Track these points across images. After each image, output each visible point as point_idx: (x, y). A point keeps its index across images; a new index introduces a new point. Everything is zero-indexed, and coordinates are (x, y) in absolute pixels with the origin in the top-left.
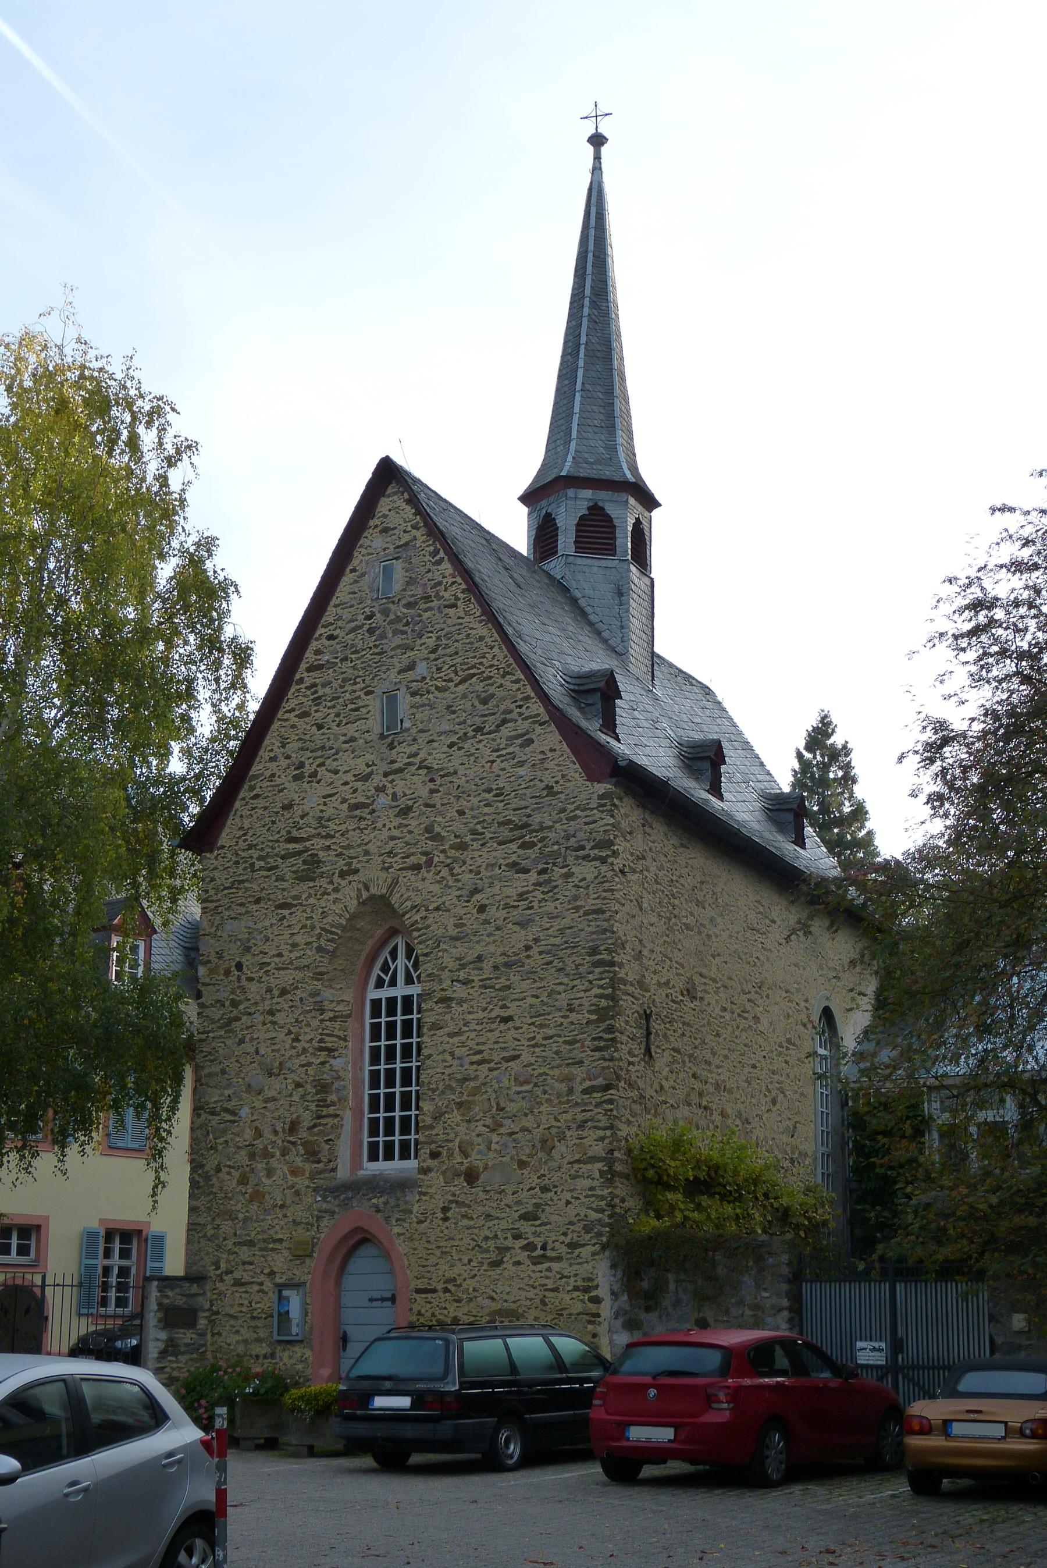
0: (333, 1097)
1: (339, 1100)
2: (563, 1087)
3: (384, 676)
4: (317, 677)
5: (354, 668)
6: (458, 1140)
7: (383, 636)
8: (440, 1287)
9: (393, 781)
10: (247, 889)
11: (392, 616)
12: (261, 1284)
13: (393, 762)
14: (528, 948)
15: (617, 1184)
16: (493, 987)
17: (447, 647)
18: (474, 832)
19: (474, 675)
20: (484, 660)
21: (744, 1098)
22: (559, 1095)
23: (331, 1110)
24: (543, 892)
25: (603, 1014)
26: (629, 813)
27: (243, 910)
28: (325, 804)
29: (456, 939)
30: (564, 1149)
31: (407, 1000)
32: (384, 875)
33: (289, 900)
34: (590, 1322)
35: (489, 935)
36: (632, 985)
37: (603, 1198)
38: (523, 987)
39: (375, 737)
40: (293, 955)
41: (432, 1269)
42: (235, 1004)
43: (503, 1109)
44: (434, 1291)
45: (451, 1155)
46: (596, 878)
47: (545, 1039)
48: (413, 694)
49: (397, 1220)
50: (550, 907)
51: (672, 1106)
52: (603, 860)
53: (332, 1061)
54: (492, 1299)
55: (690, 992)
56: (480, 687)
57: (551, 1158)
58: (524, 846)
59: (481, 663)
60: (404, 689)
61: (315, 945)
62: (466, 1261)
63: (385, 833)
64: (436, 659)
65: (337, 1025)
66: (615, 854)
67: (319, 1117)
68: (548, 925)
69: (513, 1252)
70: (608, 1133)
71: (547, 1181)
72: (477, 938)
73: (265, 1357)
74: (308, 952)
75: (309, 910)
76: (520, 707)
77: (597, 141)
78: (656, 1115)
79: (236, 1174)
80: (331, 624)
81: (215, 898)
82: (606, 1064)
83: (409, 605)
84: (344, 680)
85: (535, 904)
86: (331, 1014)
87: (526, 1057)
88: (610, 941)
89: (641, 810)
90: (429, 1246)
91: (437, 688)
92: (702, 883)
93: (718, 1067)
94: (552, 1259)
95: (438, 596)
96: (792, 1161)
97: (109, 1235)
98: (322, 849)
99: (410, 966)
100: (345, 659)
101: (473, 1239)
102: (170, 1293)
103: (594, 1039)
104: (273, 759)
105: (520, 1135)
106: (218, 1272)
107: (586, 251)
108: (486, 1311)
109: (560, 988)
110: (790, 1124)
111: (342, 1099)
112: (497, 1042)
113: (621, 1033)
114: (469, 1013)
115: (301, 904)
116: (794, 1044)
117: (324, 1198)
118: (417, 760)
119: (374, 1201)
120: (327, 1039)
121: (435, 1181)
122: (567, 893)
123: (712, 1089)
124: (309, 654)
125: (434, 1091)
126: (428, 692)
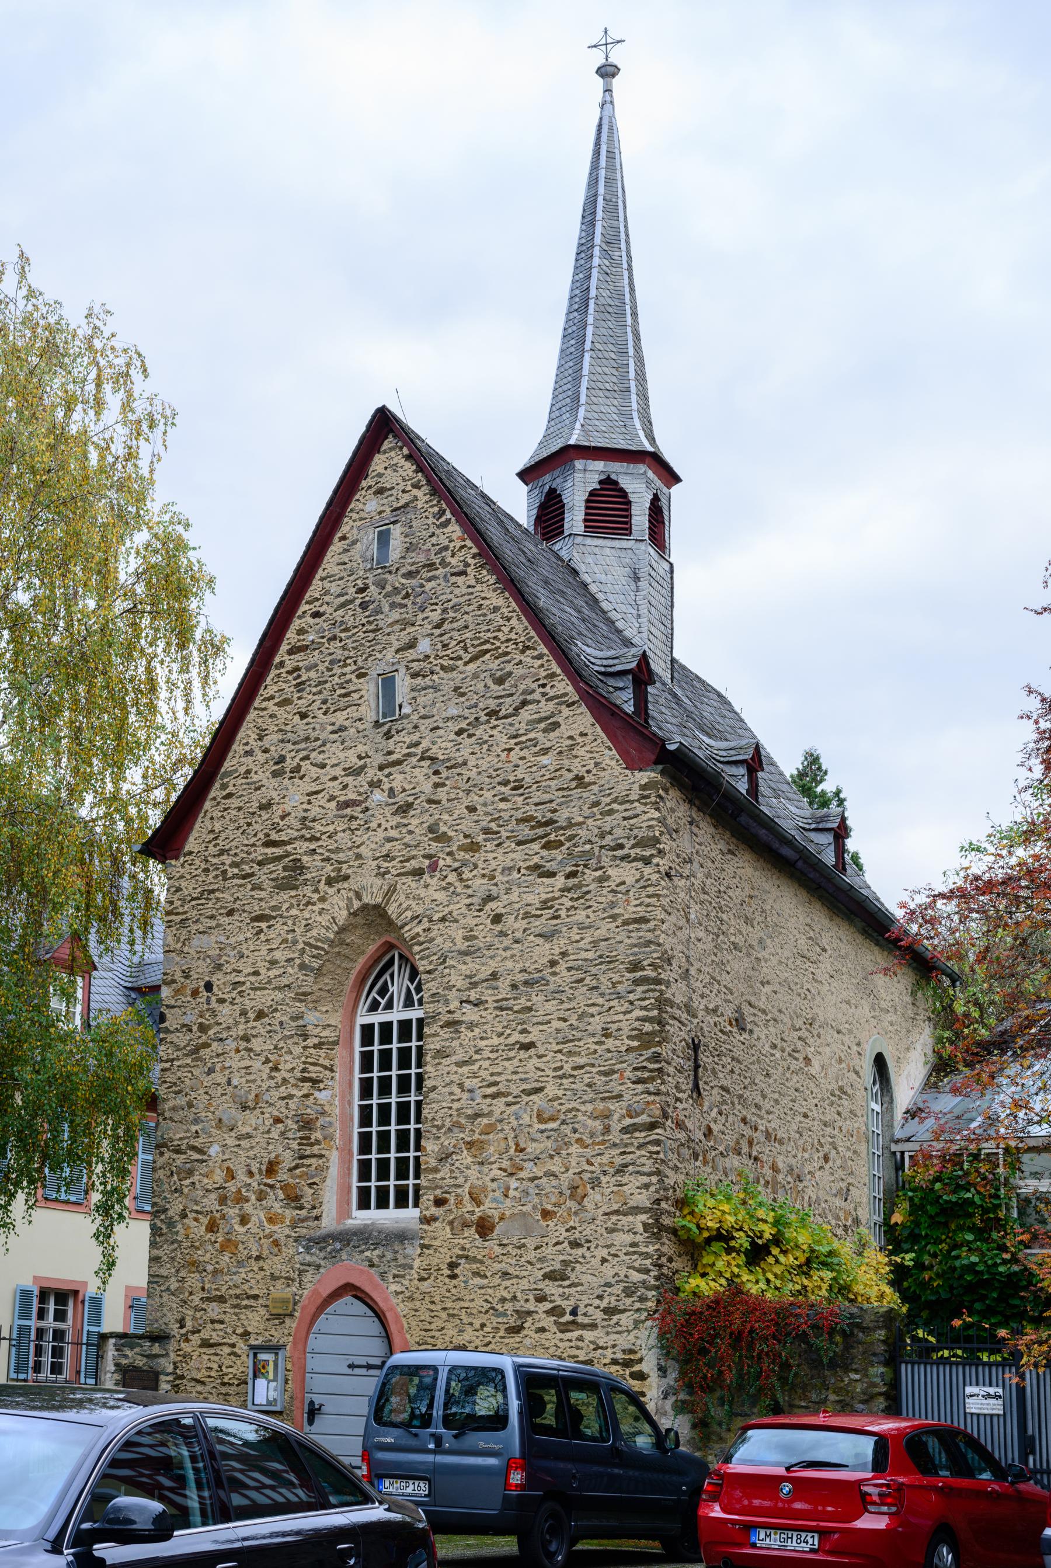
2: (597, 1125)
3: (379, 656)
5: (344, 648)
7: (378, 611)
9: (390, 774)
12: (233, 1346)
13: (390, 753)
14: (553, 963)
15: (664, 1240)
16: (510, 1009)
17: (454, 620)
18: (487, 831)
19: (487, 651)
23: (316, 1149)
26: (676, 808)
27: (214, 923)
28: (309, 802)
29: (466, 953)
31: (405, 1026)
32: (378, 882)
33: (267, 912)
37: (647, 1255)
38: (545, 1007)
39: (368, 725)
42: (203, 1028)
43: (522, 1150)
45: (459, 1203)
46: (637, 881)
47: (574, 1068)
49: (395, 1276)
50: (580, 915)
52: (647, 861)
53: (317, 1094)
55: (739, 1023)
56: (494, 665)
58: (547, 846)
60: (403, 670)
61: (298, 961)
62: (478, 1326)
63: (381, 834)
64: (442, 635)
65: (322, 1053)
67: (302, 1157)
68: (578, 937)
69: (536, 1317)
70: (654, 1179)
71: (577, 1235)
72: (491, 953)
74: (289, 970)
75: (290, 923)
76: (544, 686)
77: (607, 72)
79: (205, 1221)
81: (181, 910)
82: (651, 1098)
83: (409, 575)
86: (316, 1041)
87: (551, 1090)
88: (655, 955)
90: (433, 1307)
91: (443, 667)
93: (769, 1112)
94: (584, 1327)
95: (444, 563)
97: (44, 1295)
98: (306, 853)
99: (412, 988)
100: (334, 638)
101: (486, 1301)
102: (129, 1353)
103: (636, 1069)
105: (544, 1180)
109: (593, 1010)
110: (844, 1185)
112: (516, 1073)
113: (669, 1064)
114: (482, 1038)
115: (281, 916)
116: (845, 1093)
117: (308, 1249)
118: (418, 750)
120: (311, 1068)
122: (603, 899)
123: (763, 1139)
124: (291, 635)
125: (439, 1128)
126: (432, 673)
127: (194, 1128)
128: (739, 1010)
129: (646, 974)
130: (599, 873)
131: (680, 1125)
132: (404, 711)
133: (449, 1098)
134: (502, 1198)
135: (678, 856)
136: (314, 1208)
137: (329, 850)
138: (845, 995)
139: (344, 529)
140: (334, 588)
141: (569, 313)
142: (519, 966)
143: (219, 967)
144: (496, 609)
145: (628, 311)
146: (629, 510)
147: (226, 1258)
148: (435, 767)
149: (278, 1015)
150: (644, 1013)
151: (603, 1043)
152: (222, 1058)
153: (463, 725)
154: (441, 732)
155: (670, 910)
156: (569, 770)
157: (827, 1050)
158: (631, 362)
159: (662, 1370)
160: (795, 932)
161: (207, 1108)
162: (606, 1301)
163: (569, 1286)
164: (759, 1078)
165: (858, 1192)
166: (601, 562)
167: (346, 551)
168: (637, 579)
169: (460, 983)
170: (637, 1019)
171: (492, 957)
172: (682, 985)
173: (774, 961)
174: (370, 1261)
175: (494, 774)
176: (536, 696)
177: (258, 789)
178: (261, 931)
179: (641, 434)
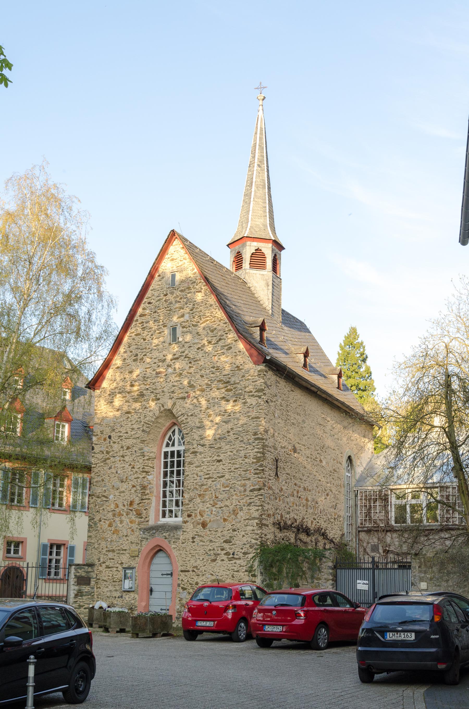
2: (242, 489)
7: (171, 303)
12: (117, 568)
15: (263, 528)
19: (208, 320)
20: (212, 314)
23: (147, 497)
25: (258, 459)
26: (271, 376)
30: (242, 514)
36: (270, 447)
37: (258, 534)
42: (108, 452)
43: (217, 497)
44: (188, 571)
46: (256, 404)
47: (235, 469)
48: (183, 327)
52: (260, 397)
53: (148, 477)
54: (212, 575)
61: (141, 429)
62: (201, 559)
63: (171, 384)
70: (260, 508)
71: (235, 527)
73: (119, 597)
74: (139, 432)
75: (139, 415)
78: (280, 500)
79: (108, 522)
82: (260, 480)
83: (182, 291)
86: (148, 457)
87: (227, 476)
90: (186, 553)
91: (193, 325)
93: (305, 481)
94: (236, 559)
98: (145, 390)
99: (180, 438)
100: (155, 312)
101: (205, 550)
102: (80, 571)
105: (224, 508)
106: (100, 562)
107: (256, 143)
109: (241, 449)
110: (334, 504)
113: (266, 467)
114: (204, 458)
117: (144, 532)
118: (184, 354)
119: (164, 534)
120: (146, 467)
121: (189, 526)
125: (189, 489)
127: (104, 489)
128: (294, 446)
131: (270, 488)
133: (193, 479)
147: (115, 536)
149: (134, 448)
150: (257, 450)
152: (114, 463)
154: (192, 348)
155: (267, 414)
162: (244, 550)
163: (232, 545)
164: (301, 469)
170: (256, 452)
172: (272, 440)
174: (165, 537)
177: (128, 365)
178: (129, 417)
179: (270, 233)
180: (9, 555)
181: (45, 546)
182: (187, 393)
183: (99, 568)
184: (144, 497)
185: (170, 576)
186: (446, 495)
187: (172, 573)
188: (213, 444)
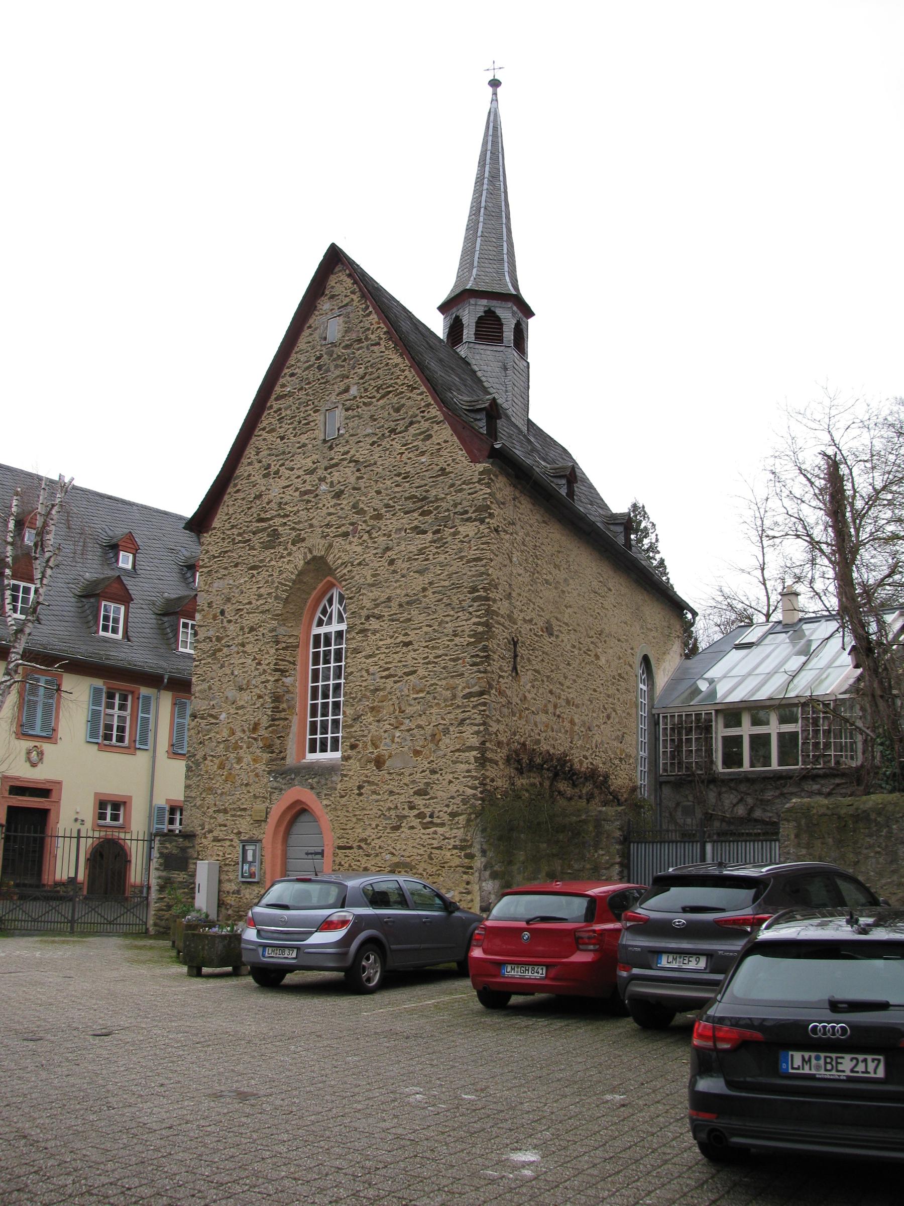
0: (284, 706)
1: (289, 708)
2: (448, 694)
3: (327, 398)
4: (282, 404)
5: (307, 394)
6: (370, 735)
7: (328, 371)
8: (355, 845)
9: (331, 472)
10: (229, 557)
11: (335, 356)
12: (231, 840)
13: (332, 459)
14: (424, 590)
15: (488, 767)
16: (398, 620)
17: (372, 373)
18: (387, 506)
19: (390, 392)
20: (398, 381)
21: (587, 712)
22: (445, 700)
23: (283, 715)
24: (437, 548)
25: (478, 637)
26: (503, 487)
27: (226, 572)
28: (284, 493)
29: (372, 585)
30: (448, 741)
31: (339, 634)
32: (323, 541)
33: (257, 563)
34: (465, 873)
35: (396, 581)
36: (502, 617)
37: (476, 778)
38: (419, 618)
39: (319, 442)
40: (258, 603)
41: (350, 832)
42: (219, 639)
43: (403, 712)
44: (351, 848)
45: (365, 746)
46: (476, 534)
47: (436, 657)
48: (347, 410)
49: (326, 795)
50: (441, 558)
51: (533, 712)
52: (482, 521)
53: (284, 679)
54: (393, 854)
55: (549, 630)
56: (395, 400)
57: (439, 749)
58: (423, 514)
59: (396, 383)
60: (340, 407)
61: (274, 594)
62: (374, 826)
63: (325, 511)
64: (364, 383)
65: (288, 653)
66: (491, 515)
67: (273, 720)
68: (439, 572)
69: (409, 819)
70: (482, 728)
71: (435, 766)
72: (387, 584)
73: (233, 893)
74: (269, 600)
75: (270, 570)
76: (423, 412)
77: (495, 84)
78: (520, 718)
79: (217, 761)
80: (293, 365)
81: (208, 565)
82: (482, 675)
83: (347, 347)
84: (300, 404)
85: (431, 557)
86: (284, 645)
87: (421, 672)
88: (485, 582)
89: (512, 489)
90: (347, 814)
91: (364, 404)
92: (559, 552)
93: (568, 687)
94: (437, 825)
95: (367, 339)
96: (621, 760)
97: (172, 811)
98: (281, 525)
99: (341, 609)
100: (301, 389)
101: (379, 810)
102: (168, 845)
103: (472, 657)
104: (250, 464)
105: (415, 731)
106: (203, 831)
107: (486, 150)
108: (388, 863)
109: (448, 619)
110: (620, 734)
111: (291, 708)
112: (400, 661)
113: (494, 653)
114: (381, 640)
115: (265, 566)
116: (623, 678)
117: (275, 778)
118: (348, 456)
119: (310, 781)
120: (281, 663)
122: (454, 547)
123: (564, 704)
124: (278, 389)
125: (354, 699)
126: (358, 407)
127: (212, 703)
128: (548, 622)
129: (482, 595)
130: (452, 530)
131: (501, 693)
132: (341, 432)
133: (360, 679)
134: (390, 744)
135: (505, 519)
136: (281, 752)
137: (294, 523)
138: (623, 618)
139: (311, 321)
140: (303, 358)
141: (470, 216)
142: (404, 592)
143: (228, 600)
144: (397, 365)
145: (504, 216)
146: (502, 329)
147: (229, 786)
148: (358, 467)
149: (261, 629)
150: (478, 620)
151: (453, 640)
152: (228, 658)
153: (375, 439)
154: (361, 444)
155: (497, 553)
156: (437, 465)
157: (611, 651)
158: (505, 244)
159: (484, 852)
160: (590, 577)
161: (219, 690)
162: (451, 808)
163: (429, 799)
164: (562, 666)
165: (630, 738)
166: (484, 359)
167: (311, 334)
168: (506, 369)
169: (369, 605)
170: (474, 624)
171: (388, 587)
172: (506, 603)
173: (575, 593)
174: (311, 785)
175: (392, 469)
176: (419, 418)
177: (254, 486)
178: (253, 576)
179: (510, 285)
180: (102, 822)
181: (161, 809)
182: (352, 524)
183: (203, 840)
184: (278, 716)
185: (319, 856)
186: (813, 718)
187: (323, 850)
188: (396, 614)
